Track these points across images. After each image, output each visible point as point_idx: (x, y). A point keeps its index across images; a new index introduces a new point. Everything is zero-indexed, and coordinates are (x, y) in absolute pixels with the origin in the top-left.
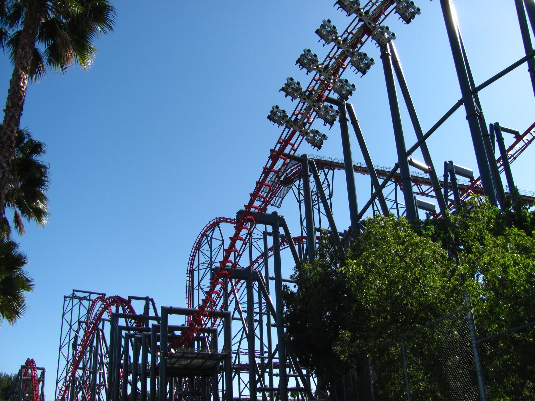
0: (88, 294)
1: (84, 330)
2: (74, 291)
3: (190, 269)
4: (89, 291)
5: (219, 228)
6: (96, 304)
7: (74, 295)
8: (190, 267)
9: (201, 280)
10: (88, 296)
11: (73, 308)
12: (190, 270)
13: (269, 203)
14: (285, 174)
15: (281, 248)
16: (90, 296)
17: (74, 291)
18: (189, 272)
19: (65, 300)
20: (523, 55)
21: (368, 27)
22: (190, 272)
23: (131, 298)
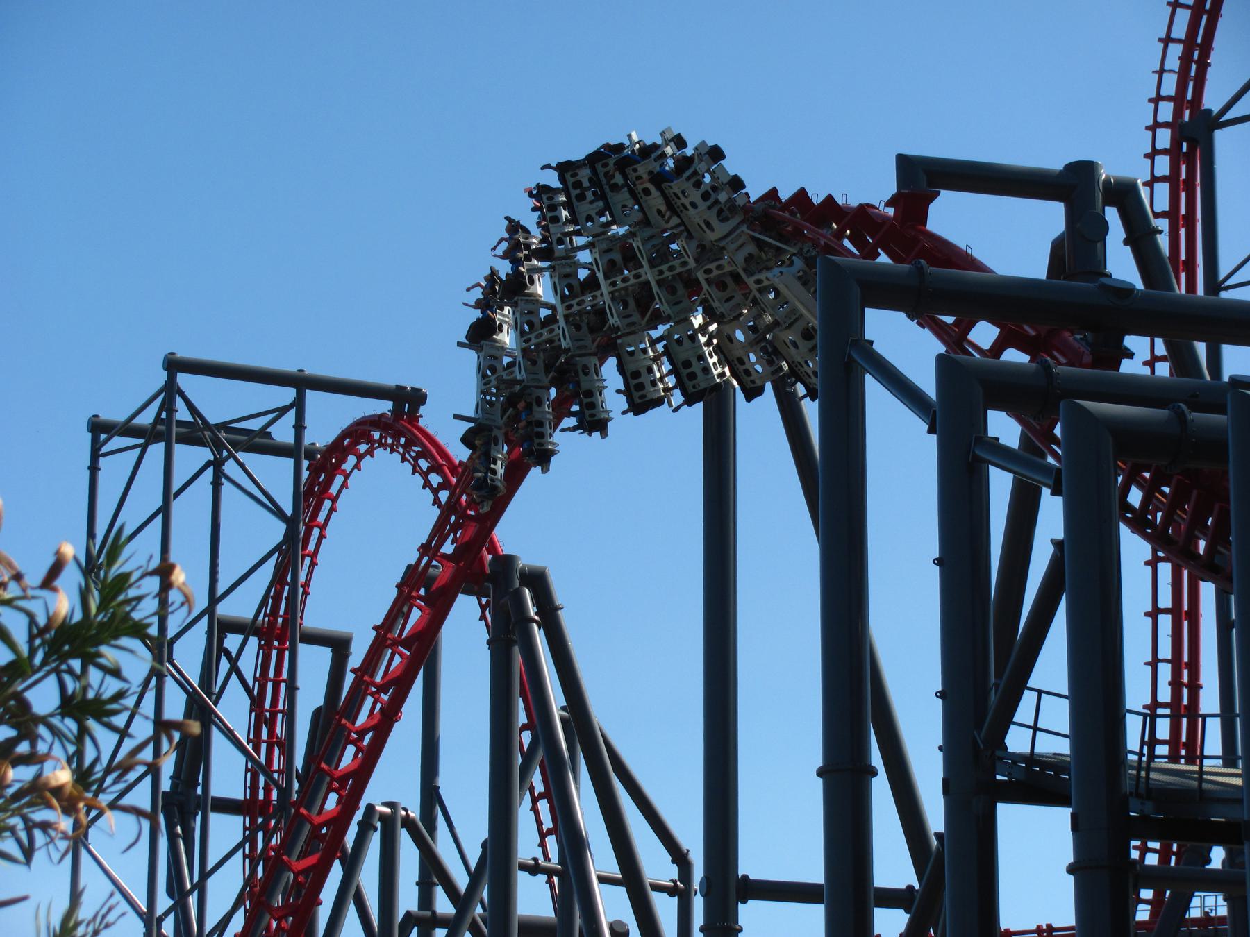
0: (286, 395)
1: (249, 691)
2: (174, 365)
3: (1178, 113)
6: (339, 479)
7: (183, 414)
8: (1178, 100)
10: (282, 411)
11: (176, 505)
12: (1175, 125)
17: (174, 365)
19: (96, 455)
21: (630, 166)
22: (1176, 143)
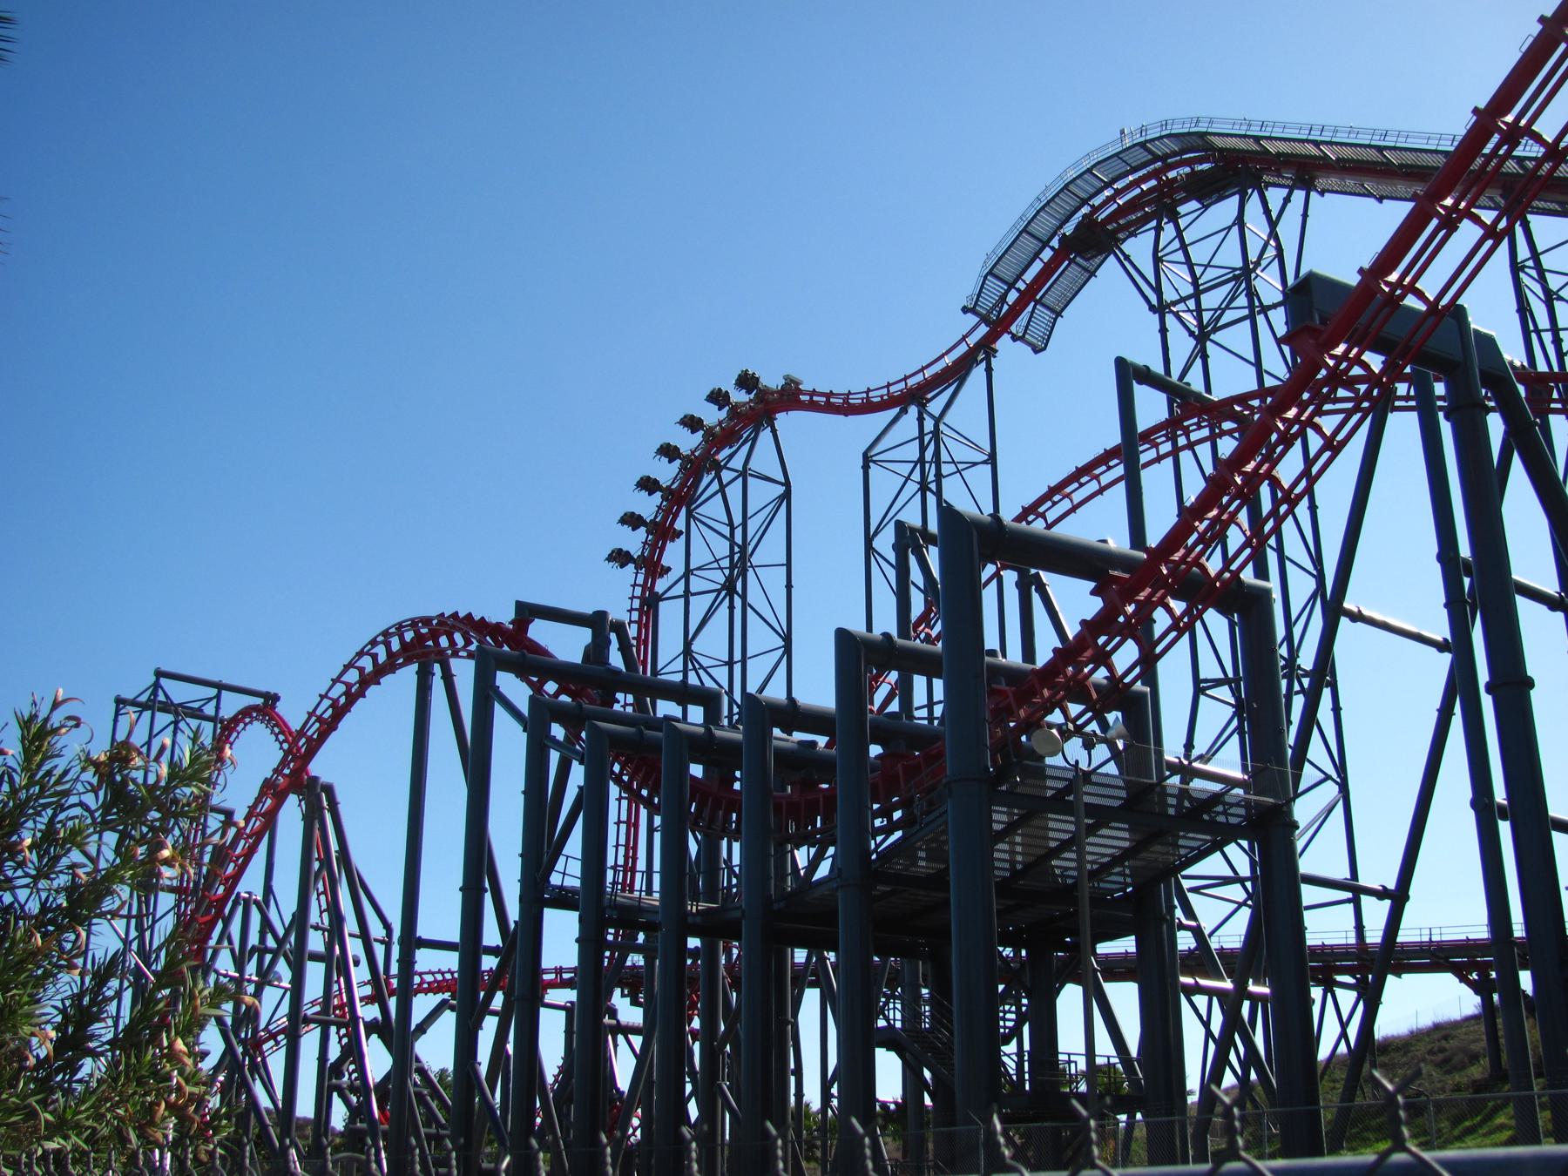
0: (213, 692)
2: (159, 674)
3: (643, 592)
4: (216, 679)
5: (774, 432)
6: (235, 734)
7: (161, 697)
8: (644, 587)
9: (876, 533)
10: (210, 699)
12: (642, 598)
13: (1006, 330)
14: (1085, 210)
15: (1144, 458)
16: (218, 697)
17: (159, 674)
18: (636, 604)
19: (117, 714)
20: (1183, 295)
22: (642, 605)
23: (527, 612)
